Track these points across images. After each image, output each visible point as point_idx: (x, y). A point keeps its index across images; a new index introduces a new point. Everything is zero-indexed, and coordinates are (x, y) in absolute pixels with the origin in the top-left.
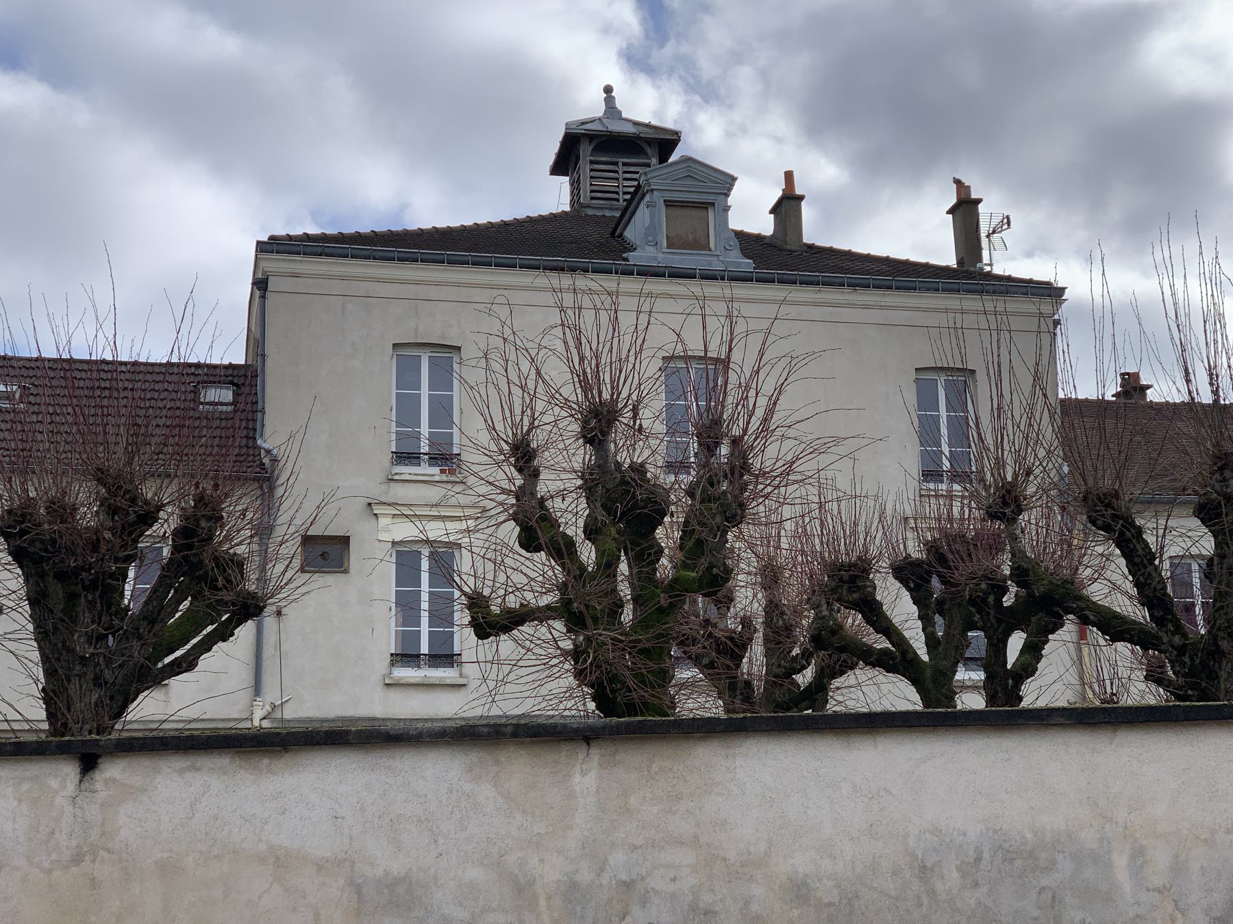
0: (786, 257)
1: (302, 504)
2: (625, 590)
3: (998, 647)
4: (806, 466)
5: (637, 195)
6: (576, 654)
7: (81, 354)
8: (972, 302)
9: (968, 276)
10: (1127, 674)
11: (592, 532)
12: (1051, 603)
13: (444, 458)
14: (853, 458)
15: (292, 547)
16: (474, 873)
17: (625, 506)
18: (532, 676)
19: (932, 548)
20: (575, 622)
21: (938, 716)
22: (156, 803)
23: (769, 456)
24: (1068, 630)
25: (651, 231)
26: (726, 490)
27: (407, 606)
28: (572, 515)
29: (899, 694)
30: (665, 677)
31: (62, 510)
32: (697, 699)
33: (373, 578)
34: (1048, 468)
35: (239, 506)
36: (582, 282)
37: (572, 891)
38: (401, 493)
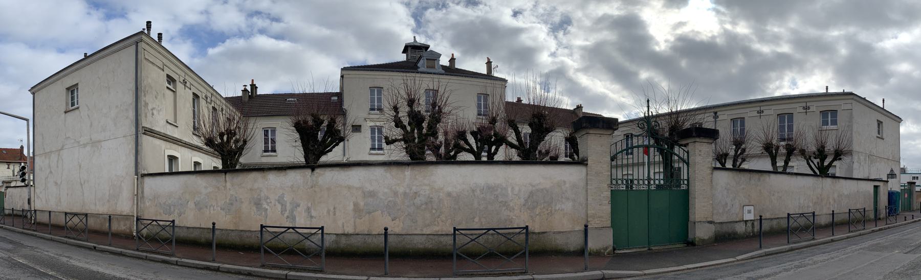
0: (451, 70)
1: (351, 119)
2: (416, 136)
3: (490, 149)
4: (453, 112)
5: (420, 57)
6: (406, 148)
7: (307, 92)
8: (489, 81)
9: (489, 76)
10: (514, 155)
11: (410, 124)
12: (501, 140)
13: (380, 109)
14: (463, 112)
15: (350, 127)
16: (386, 190)
17: (416, 118)
18: (397, 153)
19: (479, 129)
20: (406, 142)
21: (478, 162)
22: (326, 177)
23: (446, 110)
24: (504, 146)
25: (423, 64)
26: (437, 116)
27: (373, 139)
28: (406, 121)
29: (471, 157)
30: (424, 153)
31: (305, 122)
32: (430, 157)
33: (366, 133)
34: (502, 115)
35: (339, 120)
36: (408, 74)
37: (405, 194)
38: (371, 116)
